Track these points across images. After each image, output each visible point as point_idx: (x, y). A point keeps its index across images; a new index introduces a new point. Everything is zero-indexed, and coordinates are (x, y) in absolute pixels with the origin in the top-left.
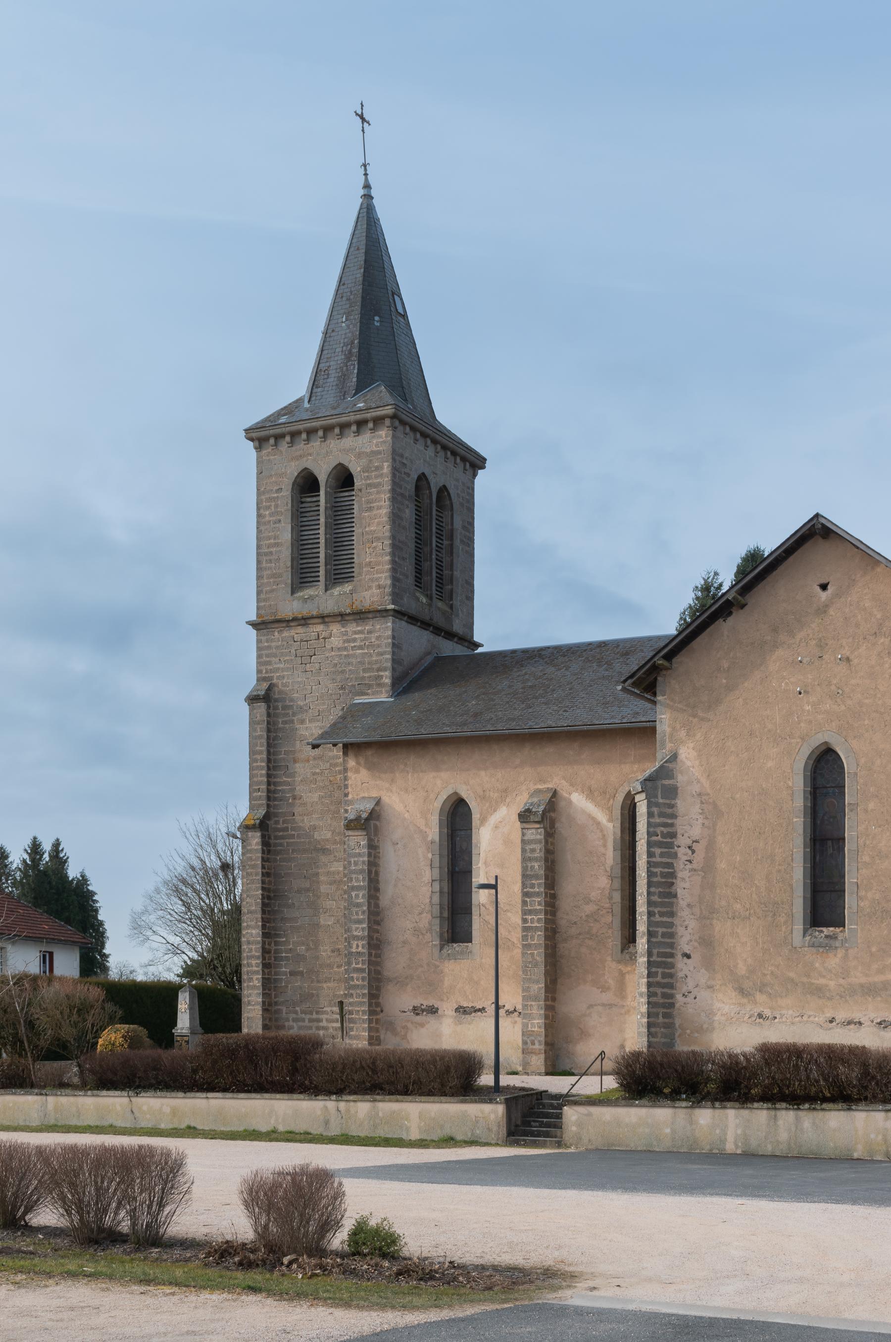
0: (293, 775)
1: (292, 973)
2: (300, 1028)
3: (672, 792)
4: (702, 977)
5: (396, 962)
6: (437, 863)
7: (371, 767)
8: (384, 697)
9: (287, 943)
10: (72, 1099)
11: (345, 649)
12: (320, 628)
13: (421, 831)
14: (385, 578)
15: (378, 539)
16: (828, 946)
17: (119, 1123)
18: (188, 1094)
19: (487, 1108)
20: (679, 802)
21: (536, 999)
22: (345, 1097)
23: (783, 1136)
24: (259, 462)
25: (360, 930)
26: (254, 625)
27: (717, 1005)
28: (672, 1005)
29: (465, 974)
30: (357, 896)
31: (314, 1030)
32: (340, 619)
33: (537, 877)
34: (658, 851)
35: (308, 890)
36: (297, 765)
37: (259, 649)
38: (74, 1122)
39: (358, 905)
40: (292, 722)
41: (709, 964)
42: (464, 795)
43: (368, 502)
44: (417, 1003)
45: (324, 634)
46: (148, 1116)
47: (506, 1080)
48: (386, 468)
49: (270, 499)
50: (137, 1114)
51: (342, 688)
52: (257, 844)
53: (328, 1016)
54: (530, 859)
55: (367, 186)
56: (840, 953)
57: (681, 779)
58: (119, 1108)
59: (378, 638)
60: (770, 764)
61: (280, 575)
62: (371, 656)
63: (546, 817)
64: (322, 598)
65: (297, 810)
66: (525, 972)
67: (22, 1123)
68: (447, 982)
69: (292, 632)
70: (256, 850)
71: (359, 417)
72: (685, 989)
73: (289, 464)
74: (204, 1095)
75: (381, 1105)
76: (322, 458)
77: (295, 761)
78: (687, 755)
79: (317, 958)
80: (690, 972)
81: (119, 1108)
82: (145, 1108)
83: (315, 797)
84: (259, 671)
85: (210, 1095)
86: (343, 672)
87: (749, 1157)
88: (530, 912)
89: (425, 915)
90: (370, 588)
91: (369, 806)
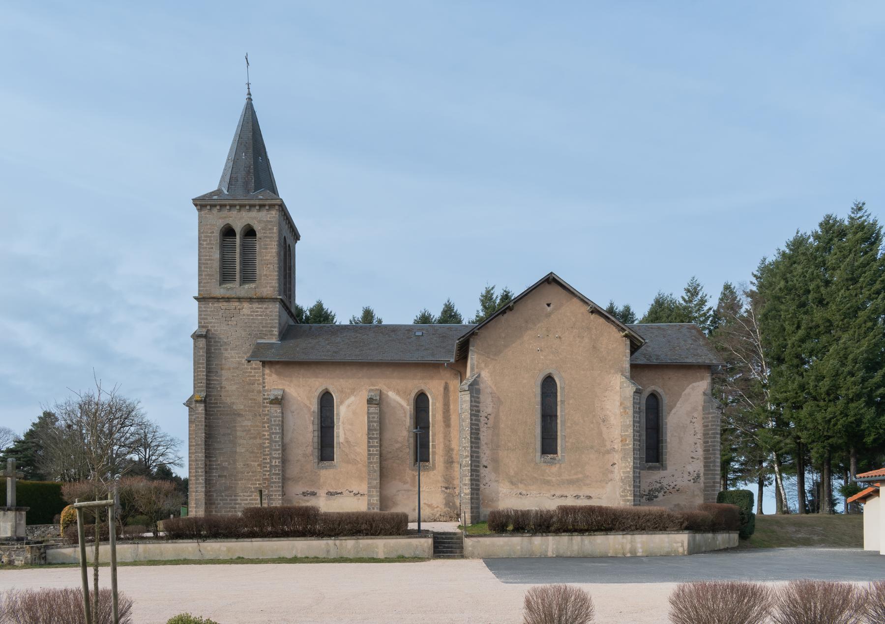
1: (219, 476)
3: (478, 391)
4: (493, 476)
5: (293, 470)
6: (316, 421)
7: (278, 374)
8: (274, 340)
9: (217, 461)
10: (157, 545)
12: (237, 304)
14: (275, 283)
15: (271, 263)
16: (552, 462)
17: (191, 557)
19: (423, 540)
20: (481, 396)
21: (375, 487)
23: (575, 548)
24: (200, 217)
25: (277, 454)
26: (196, 298)
27: (500, 489)
28: (479, 489)
29: (327, 475)
33: (375, 430)
34: (474, 418)
35: (229, 434)
37: (199, 311)
38: (158, 558)
39: (276, 442)
41: (496, 470)
44: (305, 491)
47: (424, 526)
48: (275, 229)
49: (206, 237)
55: (249, 94)
56: (558, 466)
57: (482, 386)
58: (190, 549)
60: (525, 381)
61: (212, 275)
63: (376, 402)
64: (235, 288)
65: (223, 394)
66: (369, 475)
68: (322, 480)
69: (220, 305)
71: (261, 202)
72: (484, 482)
73: (218, 220)
75: (361, 541)
76: (239, 220)
77: (222, 369)
78: (485, 374)
79: (235, 468)
80: (487, 474)
82: (209, 548)
83: (234, 388)
84: (199, 323)
85: (253, 540)
87: (560, 558)
88: (372, 447)
91: (280, 393)
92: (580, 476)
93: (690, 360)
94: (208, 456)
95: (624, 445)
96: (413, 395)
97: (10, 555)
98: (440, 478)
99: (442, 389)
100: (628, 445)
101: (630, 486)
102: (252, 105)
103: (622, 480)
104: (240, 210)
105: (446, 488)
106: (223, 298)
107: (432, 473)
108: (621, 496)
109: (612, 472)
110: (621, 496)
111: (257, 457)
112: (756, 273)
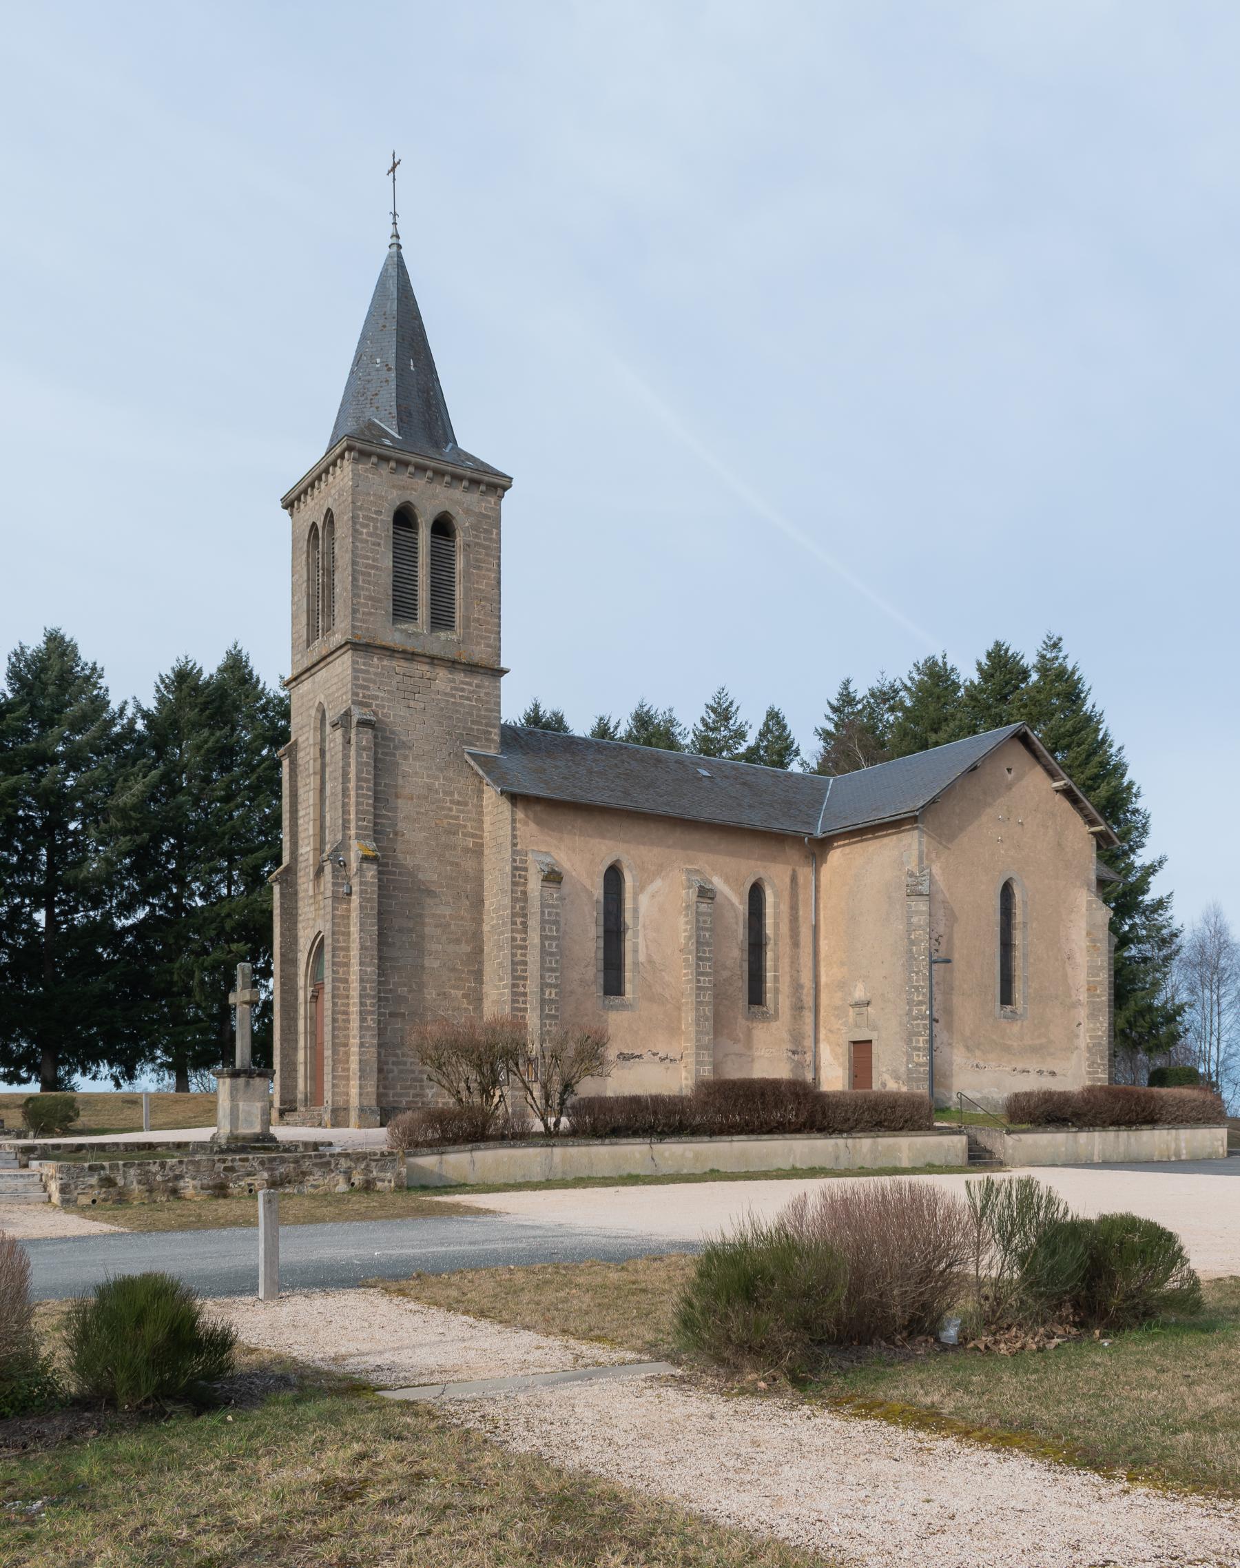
0: (395, 809)
1: (391, 1015)
2: (401, 1072)
10: (583, 1149)
11: (453, 696)
12: (426, 667)
13: (587, 891)
18: (714, 1138)
21: (707, 1048)
22: (854, 1135)
23: (1122, 1149)
30: (550, 946)
36: (399, 801)
40: (394, 755)
43: (477, 560)
51: (449, 733)
54: (703, 929)
56: (1019, 1023)
58: (638, 1156)
59: (486, 694)
61: (379, 601)
62: (479, 709)
65: (399, 847)
67: (521, 1180)
69: (394, 663)
74: (729, 1138)
77: (397, 797)
81: (638, 1156)
82: (667, 1154)
85: (735, 1138)
86: (450, 718)
88: (702, 974)
90: (478, 644)
92: (1044, 1040)
94: (382, 971)
95: (1093, 996)
96: (748, 886)
97: (367, 1170)
98: (786, 1036)
99: (788, 880)
100: (1099, 996)
101: (1102, 1058)
102: (400, 256)
103: (1089, 1049)
104: (431, 480)
105: (794, 1053)
106: (404, 652)
107: (774, 1025)
108: (1089, 1073)
109: (1077, 1036)
110: (1089, 1073)
111: (460, 979)
112: (835, 703)
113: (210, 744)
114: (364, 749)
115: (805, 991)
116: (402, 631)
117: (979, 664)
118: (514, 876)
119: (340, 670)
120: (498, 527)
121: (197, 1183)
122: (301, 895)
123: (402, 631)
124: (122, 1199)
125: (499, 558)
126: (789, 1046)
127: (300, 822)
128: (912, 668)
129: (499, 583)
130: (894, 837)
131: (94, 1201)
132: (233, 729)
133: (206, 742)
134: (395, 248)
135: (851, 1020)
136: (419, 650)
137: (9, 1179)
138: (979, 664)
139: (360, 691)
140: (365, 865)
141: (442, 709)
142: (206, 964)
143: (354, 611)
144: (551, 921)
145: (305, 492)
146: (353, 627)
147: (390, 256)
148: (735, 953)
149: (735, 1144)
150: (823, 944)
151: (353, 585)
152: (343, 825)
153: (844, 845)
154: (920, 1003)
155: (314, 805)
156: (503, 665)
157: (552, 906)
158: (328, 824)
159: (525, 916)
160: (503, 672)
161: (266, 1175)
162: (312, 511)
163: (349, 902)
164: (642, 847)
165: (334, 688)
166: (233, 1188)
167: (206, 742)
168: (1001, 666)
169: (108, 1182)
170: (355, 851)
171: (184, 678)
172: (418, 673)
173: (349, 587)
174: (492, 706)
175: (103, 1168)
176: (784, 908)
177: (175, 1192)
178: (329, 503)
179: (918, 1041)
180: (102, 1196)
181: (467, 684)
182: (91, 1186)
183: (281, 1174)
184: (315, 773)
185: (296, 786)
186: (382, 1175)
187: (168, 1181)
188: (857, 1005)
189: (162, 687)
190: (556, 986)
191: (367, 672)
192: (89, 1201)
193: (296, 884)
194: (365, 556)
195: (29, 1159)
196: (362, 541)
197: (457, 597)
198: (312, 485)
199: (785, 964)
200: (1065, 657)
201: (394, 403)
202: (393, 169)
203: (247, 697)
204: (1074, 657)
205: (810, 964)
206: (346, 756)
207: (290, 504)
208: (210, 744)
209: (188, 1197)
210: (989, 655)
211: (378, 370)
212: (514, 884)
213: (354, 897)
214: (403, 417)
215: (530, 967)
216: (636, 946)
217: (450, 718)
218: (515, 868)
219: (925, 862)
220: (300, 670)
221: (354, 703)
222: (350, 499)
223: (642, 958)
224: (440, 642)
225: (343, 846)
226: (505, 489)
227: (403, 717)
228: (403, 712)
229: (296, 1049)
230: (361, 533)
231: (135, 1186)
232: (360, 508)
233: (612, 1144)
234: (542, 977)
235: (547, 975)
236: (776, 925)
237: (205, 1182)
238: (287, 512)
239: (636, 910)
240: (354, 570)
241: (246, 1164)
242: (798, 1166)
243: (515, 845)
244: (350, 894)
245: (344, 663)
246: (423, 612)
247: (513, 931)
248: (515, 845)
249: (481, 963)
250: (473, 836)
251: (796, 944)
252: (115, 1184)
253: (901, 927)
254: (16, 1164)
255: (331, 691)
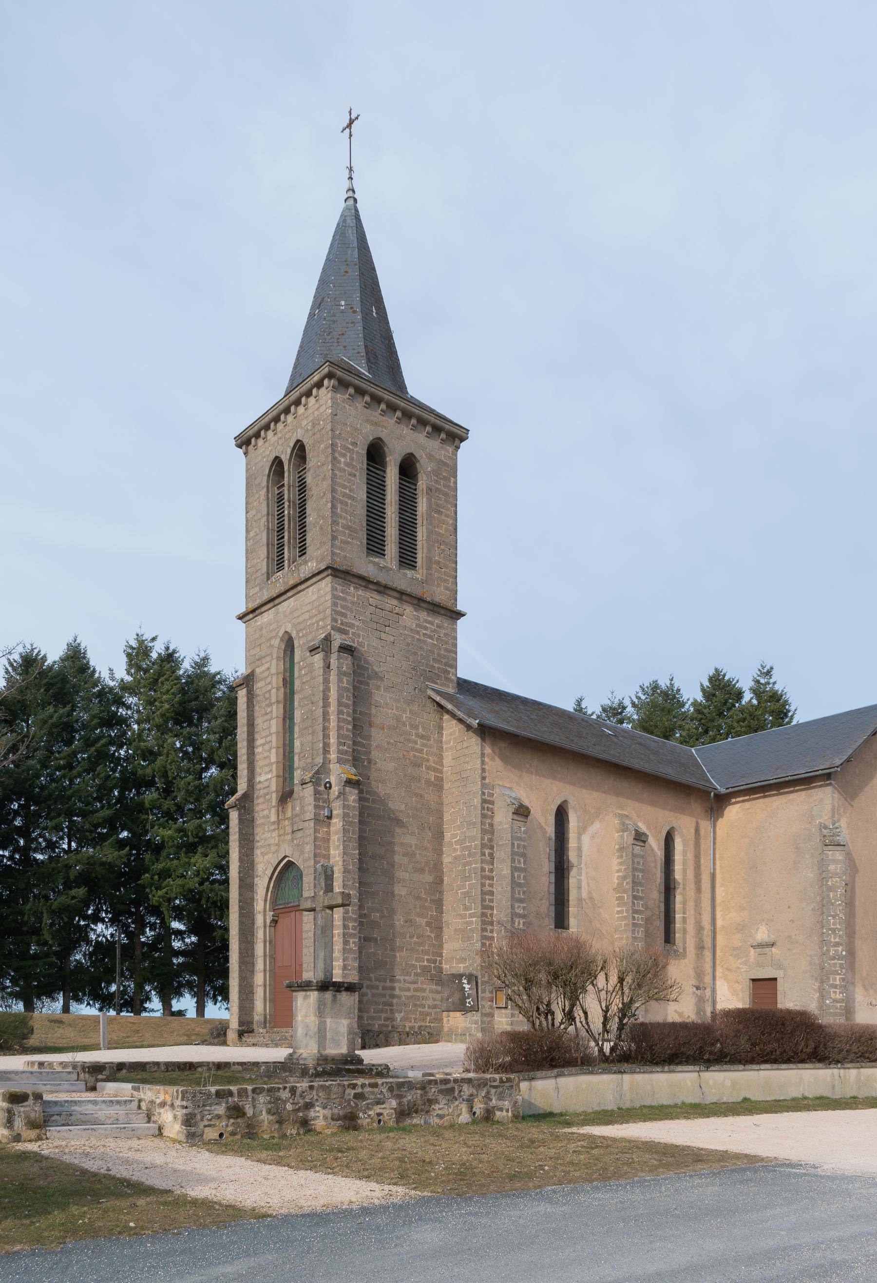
2: (374, 995)
7: (504, 759)
10: (647, 1076)
11: (418, 633)
12: (395, 602)
18: (749, 1067)
30: (519, 877)
31: (387, 997)
32: (416, 602)
36: (373, 730)
40: (368, 684)
42: (526, 802)
45: (397, 610)
46: (713, 1091)
50: (705, 1089)
51: (413, 669)
52: (354, 801)
53: (401, 985)
58: (689, 1083)
59: (446, 635)
61: (355, 531)
69: (368, 594)
70: (354, 807)
77: (371, 726)
79: (392, 926)
81: (689, 1083)
82: (711, 1082)
83: (391, 766)
85: (763, 1066)
86: (415, 654)
89: (544, 901)
90: (439, 586)
93: (636, 764)
97: (487, 1098)
98: (692, 973)
99: (693, 831)
105: (698, 988)
106: (378, 584)
113: (54, 719)
114: (345, 674)
115: (705, 933)
116: (375, 564)
117: (702, 685)
118: (483, 808)
119: (315, 597)
120: (455, 477)
121: (328, 1112)
122: (259, 821)
123: (375, 564)
124: (251, 1132)
125: (456, 506)
126: (694, 982)
127: (258, 750)
128: (639, 689)
129: (456, 529)
130: (803, 793)
131: (221, 1135)
132: (73, 710)
133: (51, 717)
134: (351, 202)
135: (752, 959)
136: (390, 584)
137: (103, 1106)
138: (702, 685)
139: (339, 618)
140: (348, 789)
141: (408, 644)
142: (53, 907)
143: (334, 538)
144: (519, 854)
145: (257, 435)
146: (333, 553)
147: (347, 208)
148: (656, 895)
149: (761, 1072)
150: (719, 890)
151: (332, 512)
152: (324, 748)
153: (743, 801)
154: (837, 944)
155: (277, 733)
156: (460, 607)
157: (520, 839)
158: (297, 750)
159: (492, 848)
160: (460, 615)
161: (394, 1103)
162: (277, 444)
163: (329, 826)
164: (584, 791)
165: (306, 616)
166: (364, 1120)
167: (51, 717)
168: (720, 689)
169: (236, 1112)
170: (337, 774)
171: (30, 662)
172: (388, 607)
173: (329, 513)
174: (450, 647)
175: (231, 1094)
176: (690, 856)
177: (305, 1123)
178: (299, 435)
179: (835, 979)
180: (230, 1129)
181: (431, 623)
182: (219, 1117)
183: (409, 1101)
184: (278, 702)
185: (253, 715)
186: (500, 1103)
187: (298, 1110)
188: (761, 945)
189: (10, 669)
190: (523, 916)
191: (344, 599)
192: (215, 1135)
193: (253, 811)
194: (334, 494)
195: (97, 1080)
196: (340, 470)
197: (419, 538)
198: (277, 419)
199: (691, 905)
200: (774, 683)
201: (361, 343)
202: (349, 126)
203: (85, 683)
204: (780, 682)
205: (709, 909)
206: (326, 681)
207: (245, 442)
208: (54, 719)
209: (319, 1129)
210: (711, 679)
211: (342, 312)
212: (484, 816)
213: (334, 821)
214: (371, 359)
215: (497, 896)
216: (579, 883)
217: (415, 654)
218: (484, 801)
219: (836, 816)
220: (258, 602)
221: (333, 628)
222: (329, 427)
223: (584, 895)
224: (404, 579)
225: (323, 769)
226: (462, 440)
227: (376, 648)
228: (375, 643)
229: (253, 972)
230: (339, 462)
231: (264, 1116)
232: (339, 437)
233: (670, 1072)
234: (512, 907)
235: (516, 905)
236: (684, 871)
237: (336, 1111)
238: (240, 452)
239: (579, 849)
240: (333, 497)
241: (376, 1090)
242: (806, 1094)
243: (484, 778)
244: (330, 817)
245: (323, 590)
246: (392, 547)
247: (482, 861)
248: (484, 778)
249: (441, 893)
250: (435, 770)
251: (699, 890)
252: (244, 1114)
253: (811, 875)
254: (81, 1085)
255: (301, 619)
